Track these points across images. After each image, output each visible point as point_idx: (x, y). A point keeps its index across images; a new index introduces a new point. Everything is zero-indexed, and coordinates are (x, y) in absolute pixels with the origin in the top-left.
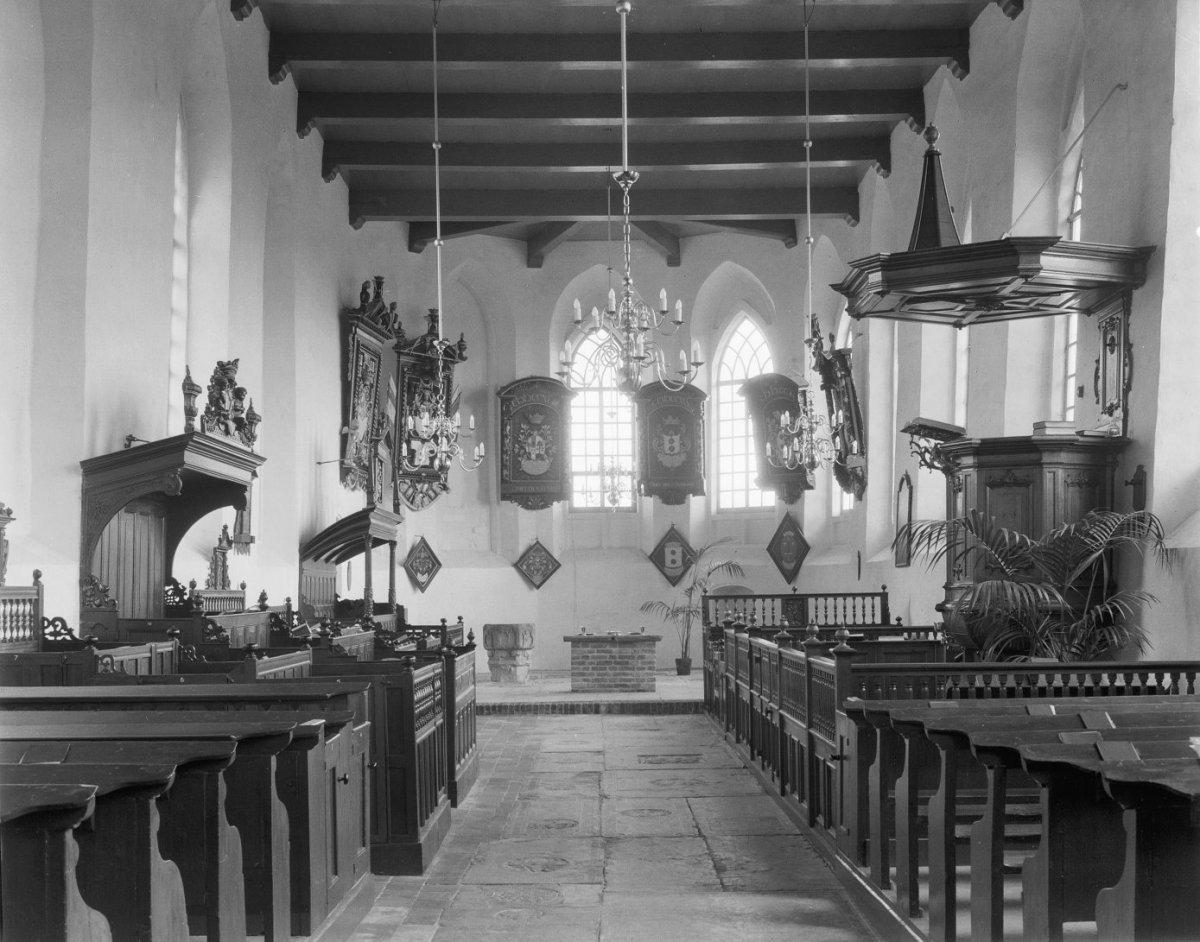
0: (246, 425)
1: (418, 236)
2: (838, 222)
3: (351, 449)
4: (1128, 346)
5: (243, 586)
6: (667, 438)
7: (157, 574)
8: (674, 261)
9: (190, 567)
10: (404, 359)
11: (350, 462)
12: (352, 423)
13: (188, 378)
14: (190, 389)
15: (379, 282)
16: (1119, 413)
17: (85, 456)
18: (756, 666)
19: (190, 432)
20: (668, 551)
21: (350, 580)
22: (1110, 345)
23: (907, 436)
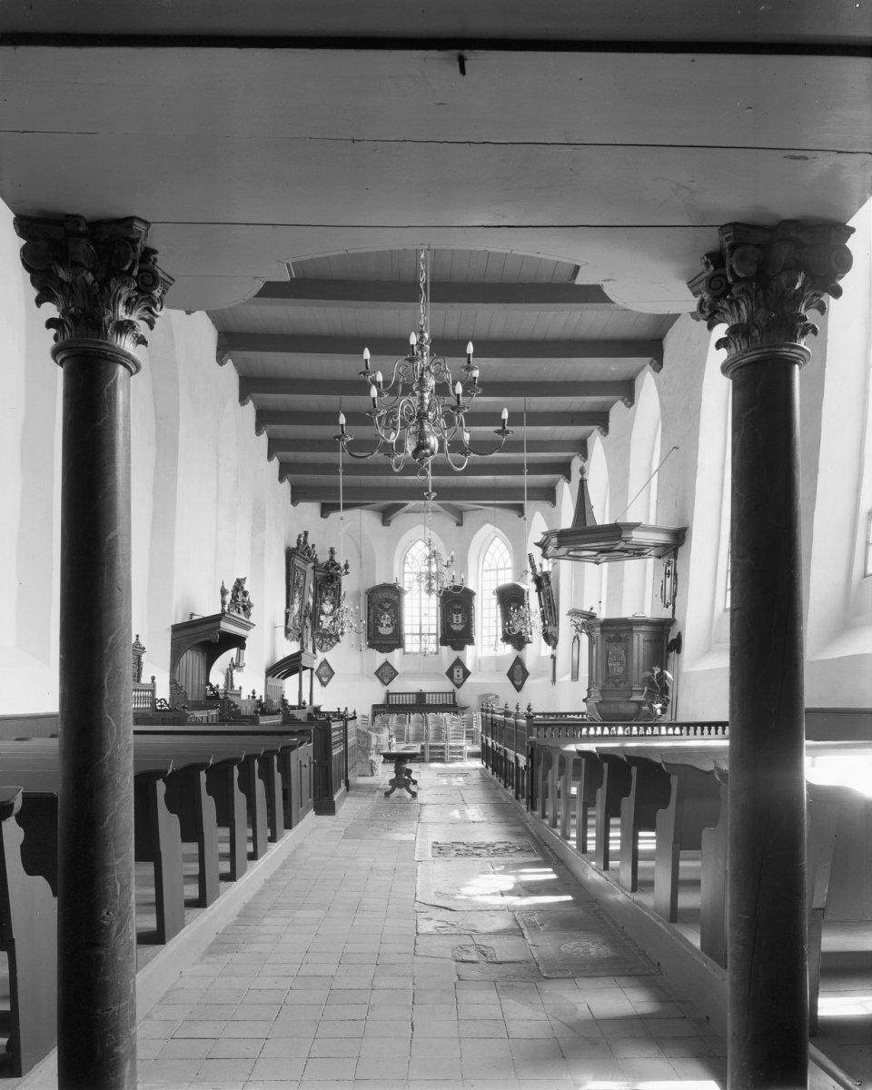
0: (246, 608)
1: (326, 510)
2: (545, 505)
3: (291, 621)
4: (676, 575)
5: (241, 688)
6: (455, 616)
7: (203, 682)
8: (460, 524)
9: (217, 678)
10: (318, 573)
11: (290, 627)
12: (291, 606)
13: (223, 586)
14: (223, 592)
15: (306, 533)
16: (671, 607)
17: (173, 624)
18: (494, 728)
19: (223, 613)
20: (455, 670)
21: (290, 689)
22: (667, 574)
23: (570, 617)
